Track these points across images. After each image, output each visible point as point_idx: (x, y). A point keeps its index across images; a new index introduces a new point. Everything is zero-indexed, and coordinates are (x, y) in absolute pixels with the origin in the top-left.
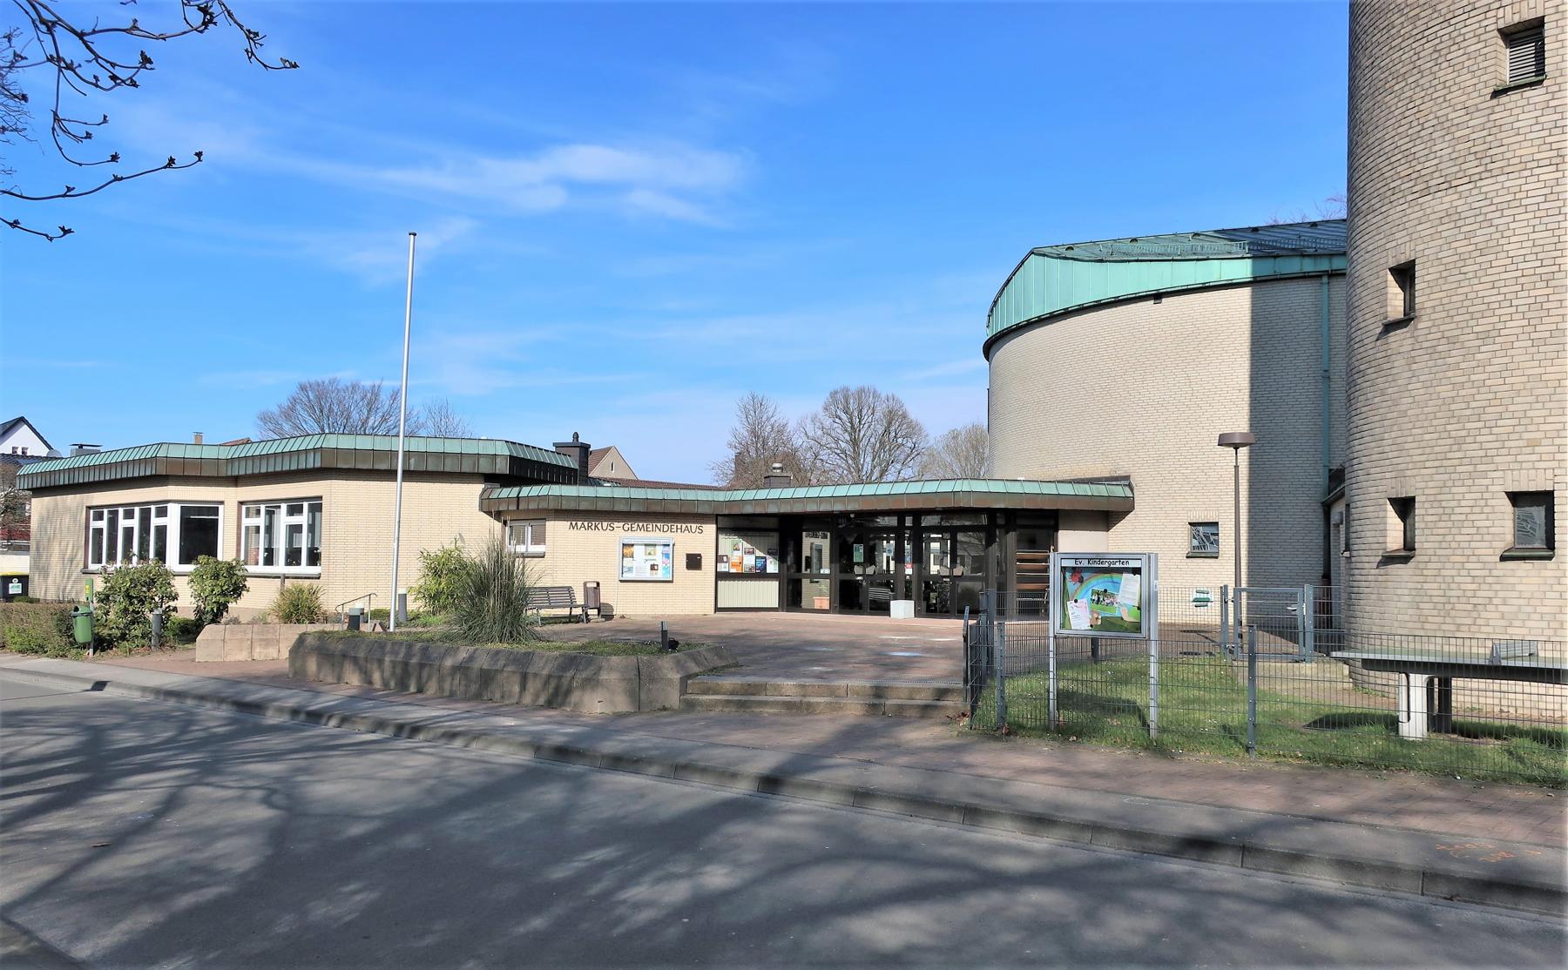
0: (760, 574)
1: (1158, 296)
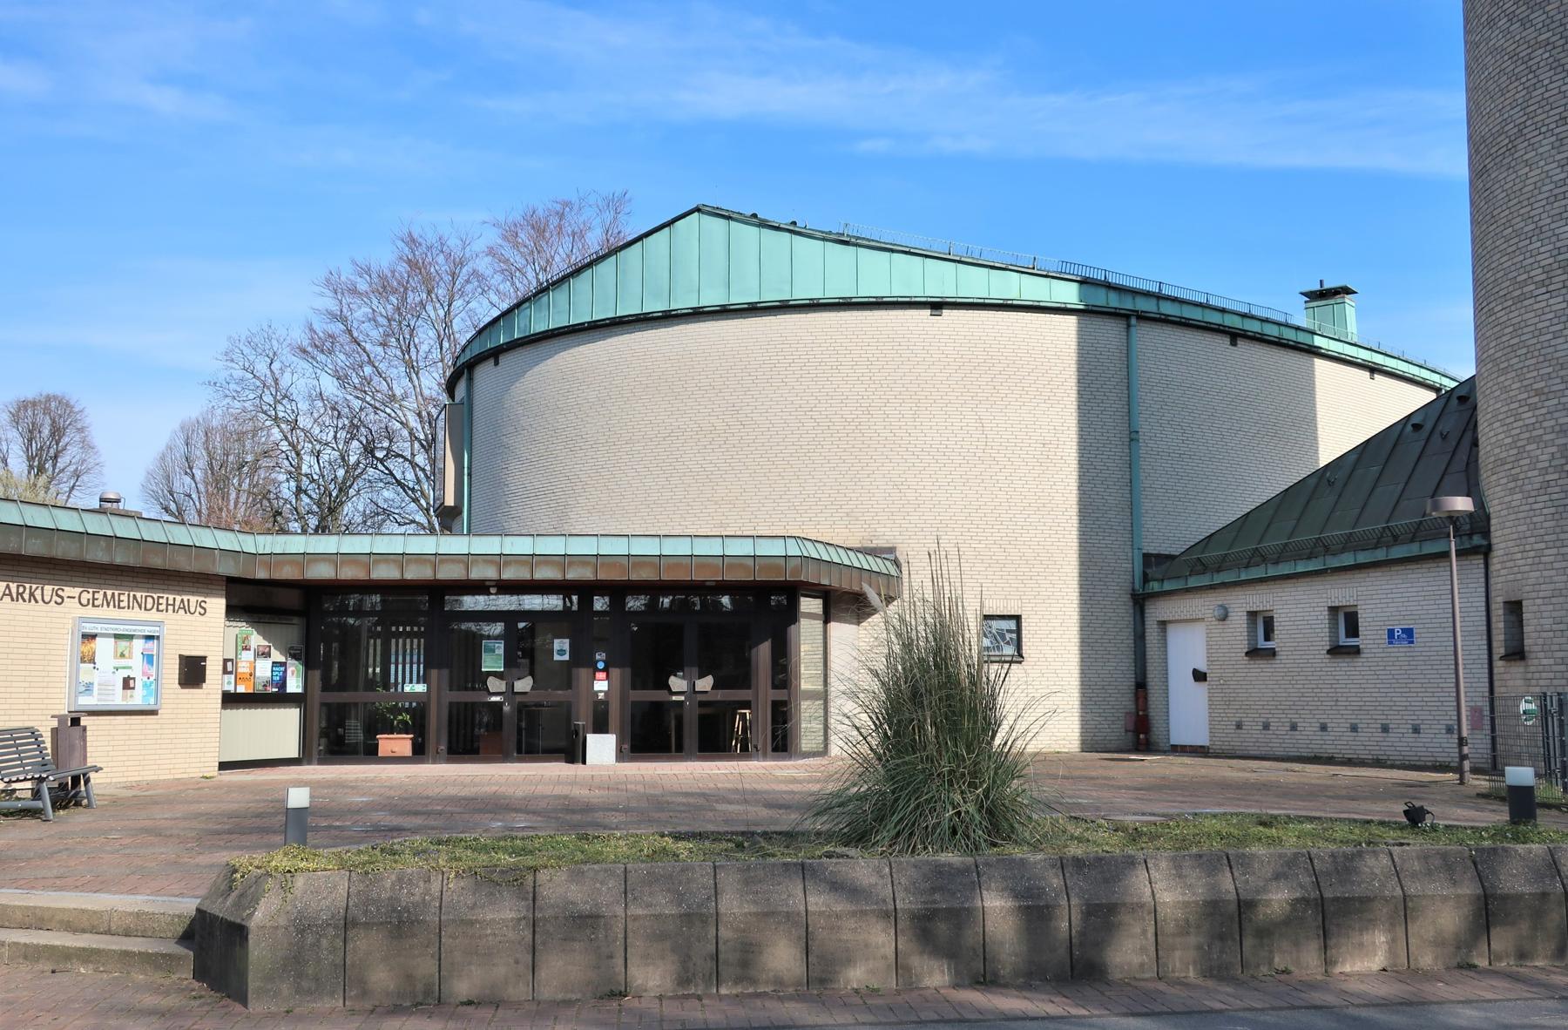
0: (275, 697)
1: (937, 306)
